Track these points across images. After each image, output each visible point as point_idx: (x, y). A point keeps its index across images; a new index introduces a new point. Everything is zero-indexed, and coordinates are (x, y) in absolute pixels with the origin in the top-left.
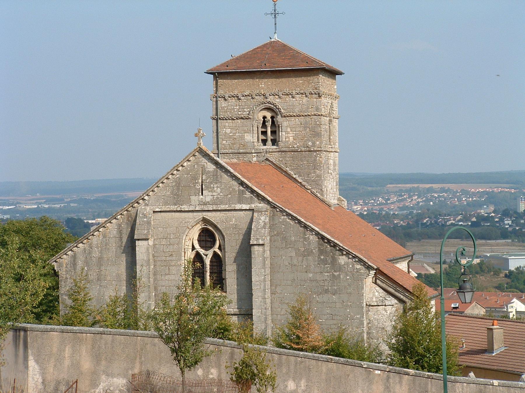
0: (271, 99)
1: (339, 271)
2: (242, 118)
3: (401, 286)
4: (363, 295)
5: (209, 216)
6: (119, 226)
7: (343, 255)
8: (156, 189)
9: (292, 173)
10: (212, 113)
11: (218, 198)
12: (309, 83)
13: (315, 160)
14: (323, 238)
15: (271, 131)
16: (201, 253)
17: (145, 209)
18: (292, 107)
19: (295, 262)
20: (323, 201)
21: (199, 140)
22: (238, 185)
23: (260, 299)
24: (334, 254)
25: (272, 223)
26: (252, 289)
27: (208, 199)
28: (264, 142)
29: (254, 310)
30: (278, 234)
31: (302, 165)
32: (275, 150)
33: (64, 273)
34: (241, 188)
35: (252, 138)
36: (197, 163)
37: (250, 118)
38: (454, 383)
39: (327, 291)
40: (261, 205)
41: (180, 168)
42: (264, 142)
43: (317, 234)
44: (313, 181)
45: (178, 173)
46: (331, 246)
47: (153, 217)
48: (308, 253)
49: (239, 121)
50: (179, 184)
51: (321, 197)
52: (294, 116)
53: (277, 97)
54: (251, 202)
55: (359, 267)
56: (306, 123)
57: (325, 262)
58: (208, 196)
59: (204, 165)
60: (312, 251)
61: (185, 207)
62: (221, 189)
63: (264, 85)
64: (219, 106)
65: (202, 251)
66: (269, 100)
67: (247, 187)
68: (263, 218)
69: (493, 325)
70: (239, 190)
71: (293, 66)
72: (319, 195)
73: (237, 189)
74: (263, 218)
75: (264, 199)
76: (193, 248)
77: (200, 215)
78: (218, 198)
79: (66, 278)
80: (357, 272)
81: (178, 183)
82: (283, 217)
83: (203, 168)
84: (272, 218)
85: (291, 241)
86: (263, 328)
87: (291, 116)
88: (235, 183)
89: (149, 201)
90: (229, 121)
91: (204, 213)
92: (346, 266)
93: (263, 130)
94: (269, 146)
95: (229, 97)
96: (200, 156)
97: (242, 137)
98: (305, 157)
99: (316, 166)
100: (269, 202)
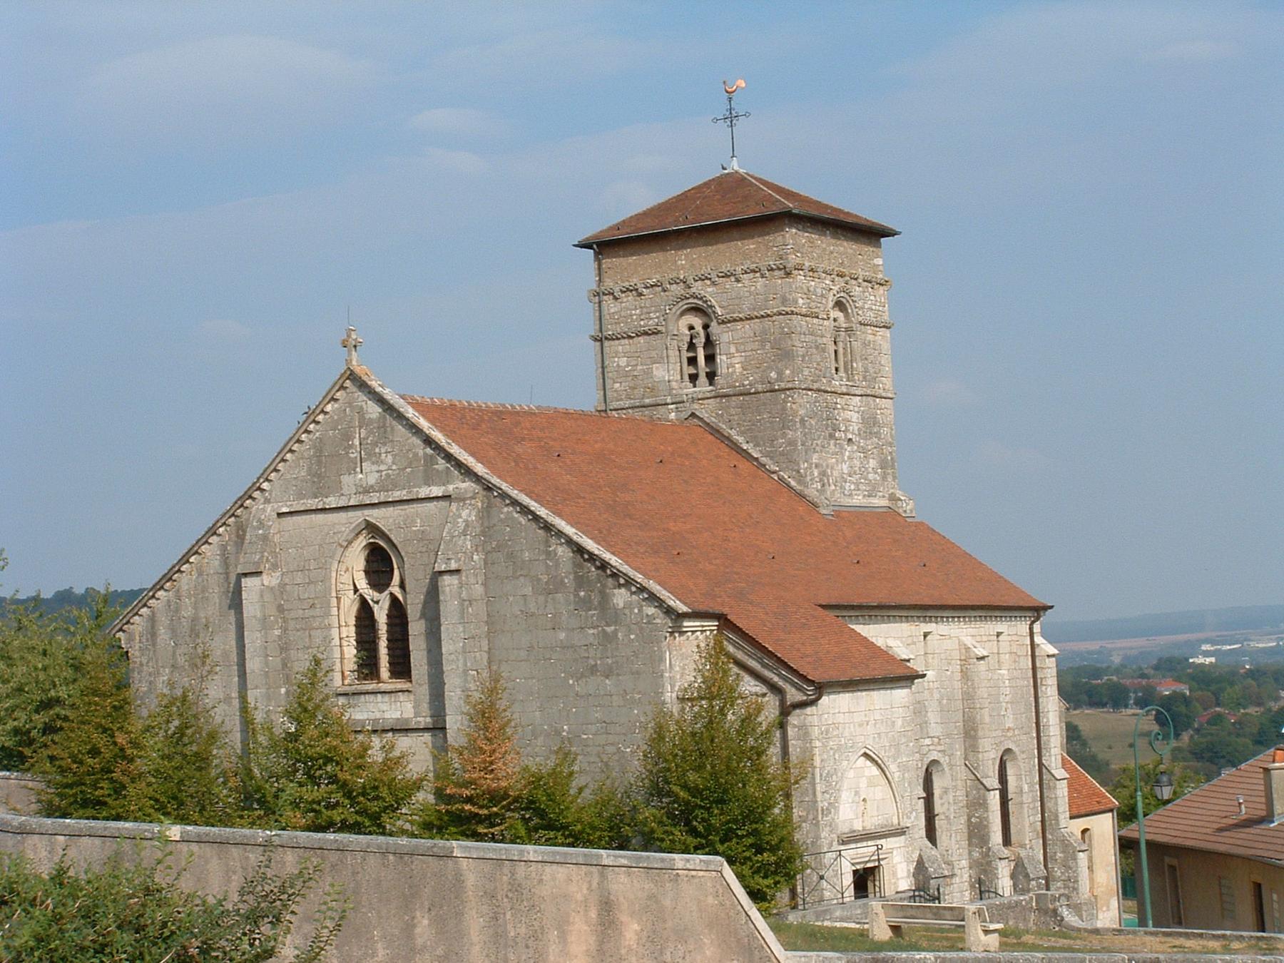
0: (697, 288)
1: (615, 623)
2: (646, 333)
3: (771, 655)
4: (662, 676)
5: (375, 516)
6: (223, 548)
7: (620, 586)
8: (280, 466)
9: (741, 439)
10: (593, 330)
11: (388, 475)
12: (768, 248)
13: (784, 409)
14: (580, 550)
15: (703, 358)
16: (368, 598)
17: (264, 510)
18: (737, 301)
19: (532, 608)
20: (801, 496)
21: (350, 353)
22: (422, 445)
23: (459, 692)
24: (604, 586)
25: (486, 524)
26: (442, 672)
27: (372, 480)
28: (693, 378)
29: (448, 718)
30: (498, 549)
31: (759, 421)
32: (708, 395)
33: (137, 653)
34: (429, 451)
35: (668, 372)
36: (350, 404)
37: (659, 332)
38: (19, 837)
39: (593, 670)
40: (464, 485)
41: (320, 418)
42: (693, 378)
43: (570, 542)
44: (782, 454)
45: (318, 427)
46: (598, 568)
47: (275, 526)
48: (556, 586)
49: (641, 339)
50: (321, 451)
51: (798, 488)
52: (741, 319)
53: (708, 282)
54: (445, 479)
55: (651, 611)
56: (764, 332)
57: (585, 604)
58: (370, 474)
59: (361, 407)
60: (562, 581)
61: (332, 502)
62: (394, 456)
63: (685, 261)
64: (605, 312)
65: (369, 594)
66: (693, 290)
67: (438, 448)
68: (464, 514)
69: (1274, 761)
70: (425, 454)
71: (730, 215)
72: (793, 483)
73: (421, 453)
74: (464, 514)
75: (468, 472)
76: (356, 590)
77: (358, 517)
78: (388, 475)
79: (141, 665)
80: (649, 623)
81: (319, 446)
82: (506, 509)
83: (361, 412)
84: (486, 513)
85: (524, 561)
86: (1166, 797)
87: (735, 320)
88: (417, 441)
89: (271, 491)
90: (623, 341)
91: (367, 512)
92: (627, 611)
93: (691, 354)
94: (703, 387)
95: (623, 292)
96: (355, 389)
97: (648, 373)
98: (764, 404)
99: (785, 422)
100: (478, 479)
